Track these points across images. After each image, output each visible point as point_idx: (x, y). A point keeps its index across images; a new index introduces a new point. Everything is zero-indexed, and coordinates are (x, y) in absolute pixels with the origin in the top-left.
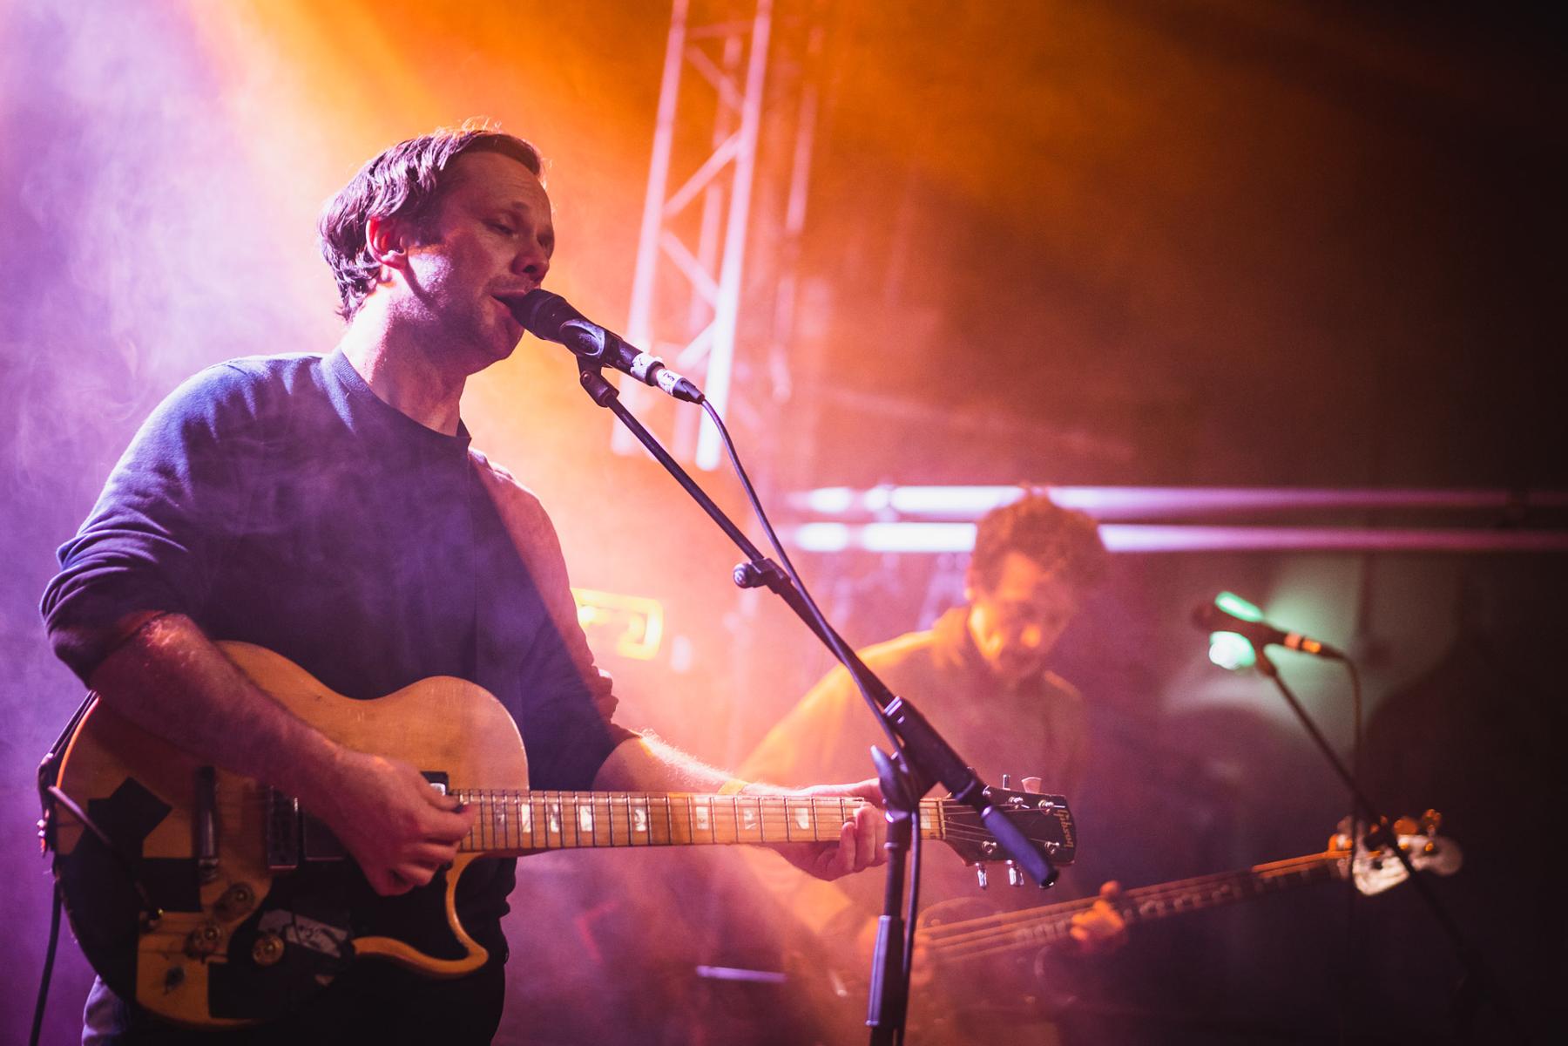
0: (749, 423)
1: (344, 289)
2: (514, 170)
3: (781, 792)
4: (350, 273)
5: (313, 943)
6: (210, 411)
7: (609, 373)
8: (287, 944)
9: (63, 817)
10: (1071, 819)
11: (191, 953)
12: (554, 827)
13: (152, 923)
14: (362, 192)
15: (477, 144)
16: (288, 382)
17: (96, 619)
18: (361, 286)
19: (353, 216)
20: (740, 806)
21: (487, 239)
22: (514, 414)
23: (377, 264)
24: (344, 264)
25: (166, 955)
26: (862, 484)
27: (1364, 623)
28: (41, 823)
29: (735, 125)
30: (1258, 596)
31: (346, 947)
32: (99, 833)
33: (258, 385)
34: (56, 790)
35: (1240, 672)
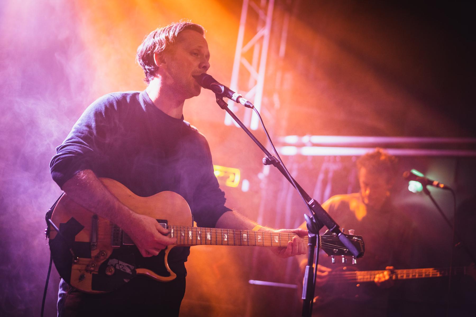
0: (267, 116)
5: (124, 269)
6: (103, 108)
7: (225, 99)
10: (363, 243)
11: (87, 270)
12: (199, 238)
16: (128, 100)
19: (149, 52)
22: (198, 111)
25: (80, 270)
26: (302, 134)
28: (46, 230)
29: (264, 24)
31: (134, 271)
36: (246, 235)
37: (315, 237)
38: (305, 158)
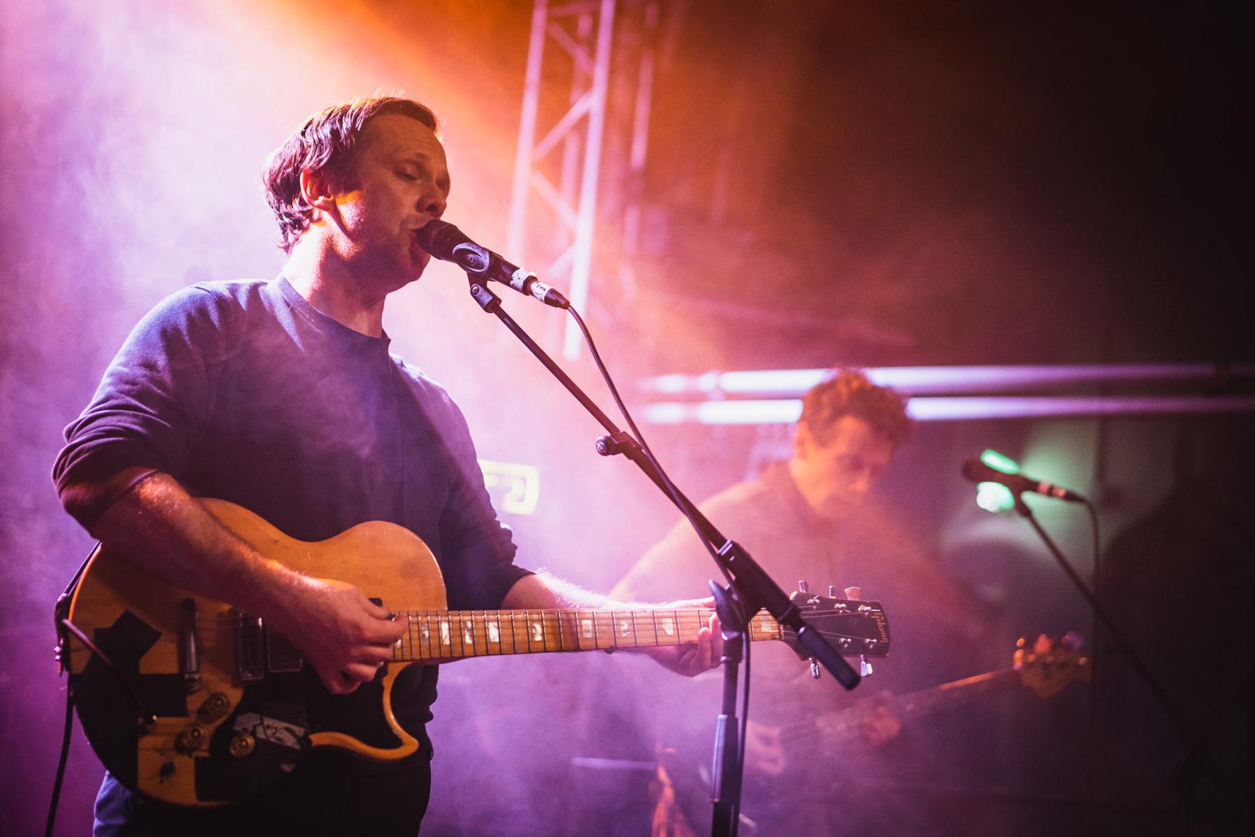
1: (284, 227)
2: (420, 126)
3: (649, 607)
4: (289, 215)
5: (278, 739)
6: (182, 322)
8: (257, 740)
9: (74, 644)
10: (885, 620)
11: (180, 749)
12: (468, 640)
13: (149, 727)
14: (295, 150)
15: (387, 107)
17: (97, 477)
18: (297, 225)
19: (290, 170)
20: (619, 619)
21: (398, 186)
22: (428, 323)
23: (310, 207)
24: (283, 208)
26: (695, 370)
27: (1101, 472)
28: (57, 649)
29: (588, 85)
30: (1015, 454)
31: (304, 741)
32: (103, 656)
33: (220, 301)
34: (67, 622)
35: (1002, 514)
36: (589, 622)
37: (740, 638)
38: (707, 430)
